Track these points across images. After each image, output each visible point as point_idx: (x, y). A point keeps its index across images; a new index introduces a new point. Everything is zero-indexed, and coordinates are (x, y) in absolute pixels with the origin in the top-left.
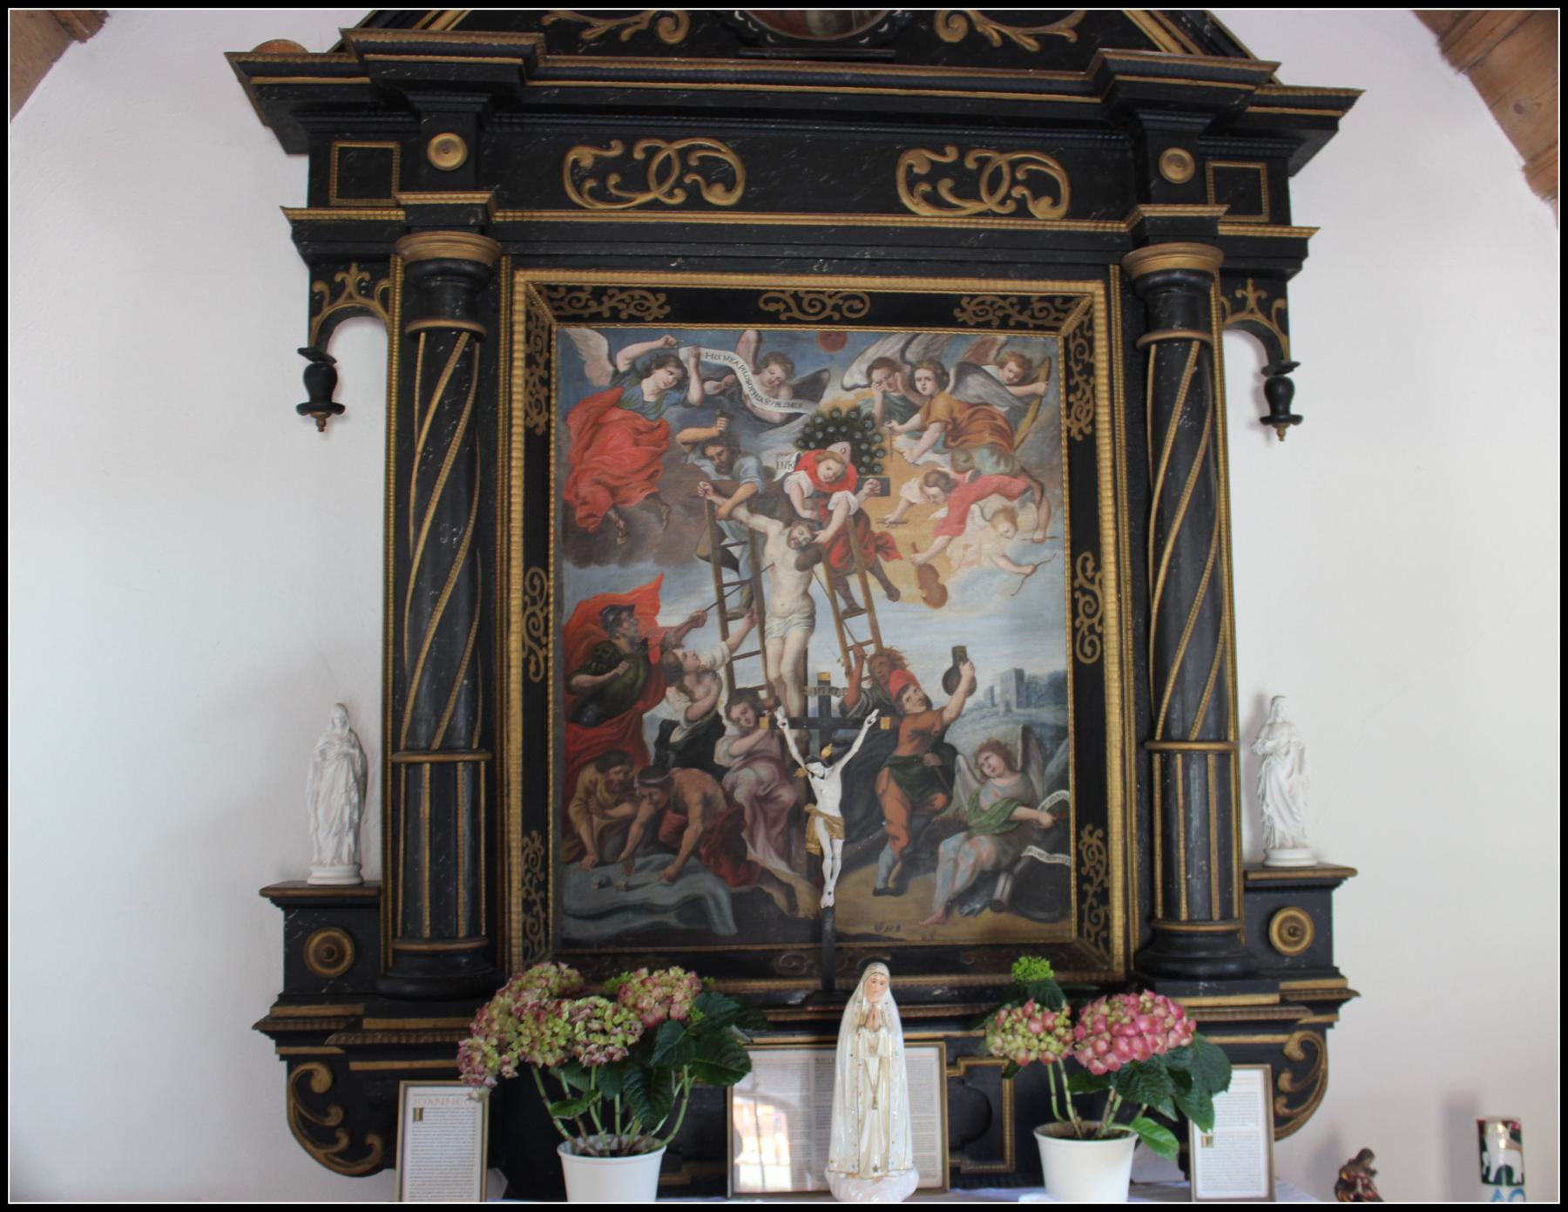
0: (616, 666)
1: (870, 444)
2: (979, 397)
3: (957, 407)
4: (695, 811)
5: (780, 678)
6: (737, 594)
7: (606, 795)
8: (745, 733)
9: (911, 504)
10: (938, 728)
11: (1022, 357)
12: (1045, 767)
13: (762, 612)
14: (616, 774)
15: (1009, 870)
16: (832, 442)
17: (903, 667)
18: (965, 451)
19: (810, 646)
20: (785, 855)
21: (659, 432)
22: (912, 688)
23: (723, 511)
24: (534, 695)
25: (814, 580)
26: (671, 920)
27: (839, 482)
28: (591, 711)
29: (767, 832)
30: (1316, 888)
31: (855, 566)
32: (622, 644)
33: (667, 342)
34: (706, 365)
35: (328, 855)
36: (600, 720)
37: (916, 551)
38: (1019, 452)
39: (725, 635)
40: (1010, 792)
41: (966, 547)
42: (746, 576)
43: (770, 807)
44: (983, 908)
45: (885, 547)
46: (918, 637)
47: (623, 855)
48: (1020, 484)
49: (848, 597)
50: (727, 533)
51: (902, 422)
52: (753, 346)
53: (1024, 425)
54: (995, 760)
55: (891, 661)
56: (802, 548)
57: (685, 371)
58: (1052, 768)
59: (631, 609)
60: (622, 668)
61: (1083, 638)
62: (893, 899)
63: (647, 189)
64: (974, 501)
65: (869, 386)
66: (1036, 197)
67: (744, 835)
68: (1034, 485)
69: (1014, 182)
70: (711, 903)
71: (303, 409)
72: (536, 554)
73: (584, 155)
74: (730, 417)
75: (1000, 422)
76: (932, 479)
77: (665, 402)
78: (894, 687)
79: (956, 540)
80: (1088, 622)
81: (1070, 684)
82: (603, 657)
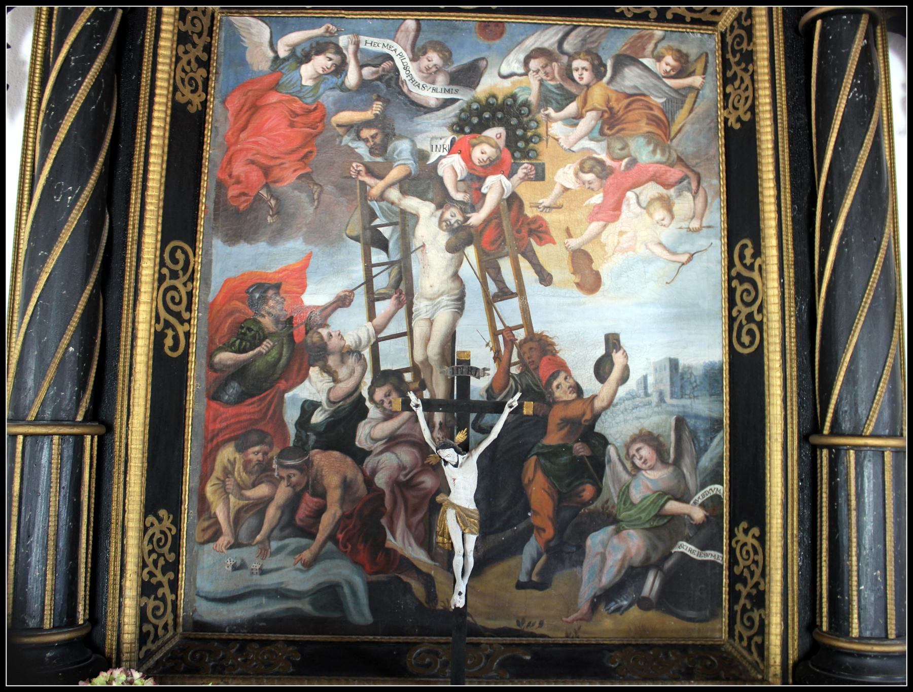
0: (260, 344)
1: (525, 130)
2: (636, 87)
3: (613, 97)
4: (334, 496)
6: (385, 274)
7: (244, 475)
8: (389, 416)
9: (566, 189)
10: (588, 416)
11: (679, 51)
13: (410, 293)
14: (255, 454)
15: (658, 566)
16: (487, 127)
17: (554, 353)
18: (621, 139)
19: (457, 329)
21: (316, 114)
22: (563, 375)
26: (305, 606)
27: (493, 166)
28: (233, 389)
31: (507, 249)
32: (267, 322)
33: (327, 30)
36: (242, 398)
37: (570, 236)
38: (675, 141)
39: (371, 315)
40: (662, 486)
41: (621, 233)
42: (395, 255)
43: (410, 494)
44: (630, 605)
45: (539, 231)
46: (571, 323)
48: (676, 173)
49: (499, 281)
50: (378, 213)
51: (559, 109)
52: (412, 35)
53: (681, 116)
54: (646, 452)
55: (542, 346)
56: (453, 230)
58: (706, 461)
59: (277, 287)
61: (741, 326)
62: (536, 593)
64: (630, 188)
65: (526, 74)
67: (384, 521)
68: (690, 174)
74: (387, 102)
75: (657, 113)
79: (611, 226)
81: (726, 375)
82: (247, 335)
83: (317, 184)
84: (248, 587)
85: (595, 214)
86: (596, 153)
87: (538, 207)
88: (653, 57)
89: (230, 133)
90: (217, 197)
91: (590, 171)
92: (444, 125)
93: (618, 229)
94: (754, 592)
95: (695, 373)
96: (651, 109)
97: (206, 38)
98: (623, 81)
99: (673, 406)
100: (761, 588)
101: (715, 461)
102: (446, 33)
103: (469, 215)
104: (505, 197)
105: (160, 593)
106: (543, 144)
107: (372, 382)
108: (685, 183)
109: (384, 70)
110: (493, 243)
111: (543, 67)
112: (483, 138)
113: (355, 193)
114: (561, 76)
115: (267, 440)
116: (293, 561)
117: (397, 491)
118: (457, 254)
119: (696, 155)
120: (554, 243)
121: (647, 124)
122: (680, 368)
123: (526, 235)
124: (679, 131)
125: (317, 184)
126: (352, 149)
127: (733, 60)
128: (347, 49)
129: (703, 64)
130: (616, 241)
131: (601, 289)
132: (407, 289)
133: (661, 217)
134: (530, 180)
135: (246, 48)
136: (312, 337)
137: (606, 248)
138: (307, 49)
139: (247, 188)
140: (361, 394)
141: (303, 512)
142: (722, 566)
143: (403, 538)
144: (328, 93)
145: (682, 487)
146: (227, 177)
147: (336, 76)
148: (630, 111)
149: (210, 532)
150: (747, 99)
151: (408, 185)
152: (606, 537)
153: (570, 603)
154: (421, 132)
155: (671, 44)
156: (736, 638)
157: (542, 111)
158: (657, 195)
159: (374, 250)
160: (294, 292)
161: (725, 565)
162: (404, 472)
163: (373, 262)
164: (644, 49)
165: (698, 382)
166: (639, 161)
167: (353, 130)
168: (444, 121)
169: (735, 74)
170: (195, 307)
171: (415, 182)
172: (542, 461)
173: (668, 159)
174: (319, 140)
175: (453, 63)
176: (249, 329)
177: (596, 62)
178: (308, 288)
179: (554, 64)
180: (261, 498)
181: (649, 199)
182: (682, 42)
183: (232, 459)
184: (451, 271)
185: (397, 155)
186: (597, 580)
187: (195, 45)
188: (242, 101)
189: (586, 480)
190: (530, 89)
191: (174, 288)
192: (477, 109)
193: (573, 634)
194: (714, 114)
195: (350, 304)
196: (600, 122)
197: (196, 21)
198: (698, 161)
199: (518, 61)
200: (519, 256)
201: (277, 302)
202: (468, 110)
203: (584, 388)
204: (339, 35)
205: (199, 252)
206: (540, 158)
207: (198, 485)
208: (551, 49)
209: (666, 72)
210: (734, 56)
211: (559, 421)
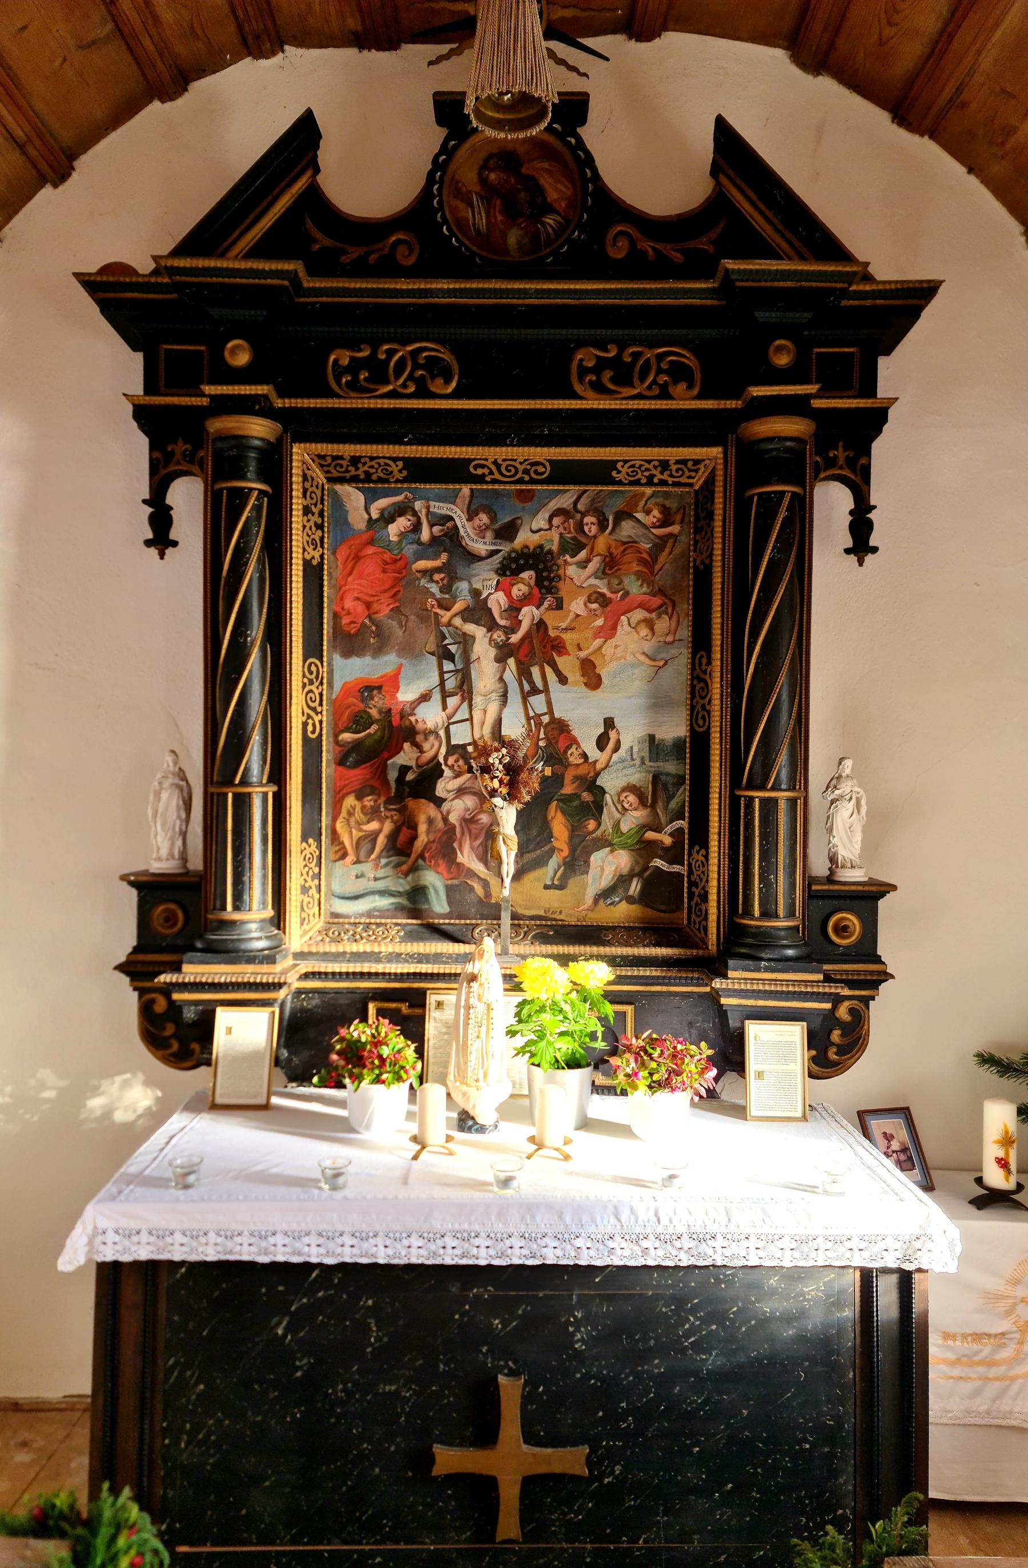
0: (369, 728)
1: (549, 572)
2: (630, 536)
3: (613, 544)
4: (422, 828)
6: (453, 678)
7: (362, 816)
8: (457, 775)
9: (578, 616)
10: (592, 774)
11: (663, 506)
12: (668, 803)
14: (369, 801)
15: (640, 875)
16: (523, 571)
17: (569, 732)
18: (618, 577)
20: (484, 860)
21: (400, 564)
22: (574, 747)
24: (312, 748)
29: (471, 844)
30: (868, 898)
32: (374, 712)
33: (406, 497)
34: (434, 514)
35: (164, 852)
37: (580, 649)
39: (445, 707)
40: (642, 821)
41: (616, 647)
42: (460, 666)
43: (473, 827)
44: (621, 901)
45: (559, 647)
46: (579, 709)
47: (373, 857)
48: (657, 601)
49: (531, 682)
53: (663, 558)
54: (632, 798)
55: (559, 728)
56: (499, 647)
57: (419, 519)
58: (673, 804)
59: (379, 688)
60: (374, 728)
61: (698, 712)
62: (557, 892)
63: (387, 382)
65: (550, 529)
66: (675, 383)
67: (455, 845)
69: (660, 371)
70: (432, 890)
71: (148, 543)
72: (313, 649)
73: (343, 357)
74: (451, 554)
75: (645, 555)
76: (593, 598)
78: (562, 745)
79: (609, 642)
82: (360, 721)
85: (598, 633)
97: (320, 506)
134: (553, 609)
141: (402, 838)
149: (340, 853)
151: (468, 615)
153: (580, 901)
170: (324, 703)
174: (404, 582)
176: (361, 717)
184: (497, 677)
205: (325, 664)
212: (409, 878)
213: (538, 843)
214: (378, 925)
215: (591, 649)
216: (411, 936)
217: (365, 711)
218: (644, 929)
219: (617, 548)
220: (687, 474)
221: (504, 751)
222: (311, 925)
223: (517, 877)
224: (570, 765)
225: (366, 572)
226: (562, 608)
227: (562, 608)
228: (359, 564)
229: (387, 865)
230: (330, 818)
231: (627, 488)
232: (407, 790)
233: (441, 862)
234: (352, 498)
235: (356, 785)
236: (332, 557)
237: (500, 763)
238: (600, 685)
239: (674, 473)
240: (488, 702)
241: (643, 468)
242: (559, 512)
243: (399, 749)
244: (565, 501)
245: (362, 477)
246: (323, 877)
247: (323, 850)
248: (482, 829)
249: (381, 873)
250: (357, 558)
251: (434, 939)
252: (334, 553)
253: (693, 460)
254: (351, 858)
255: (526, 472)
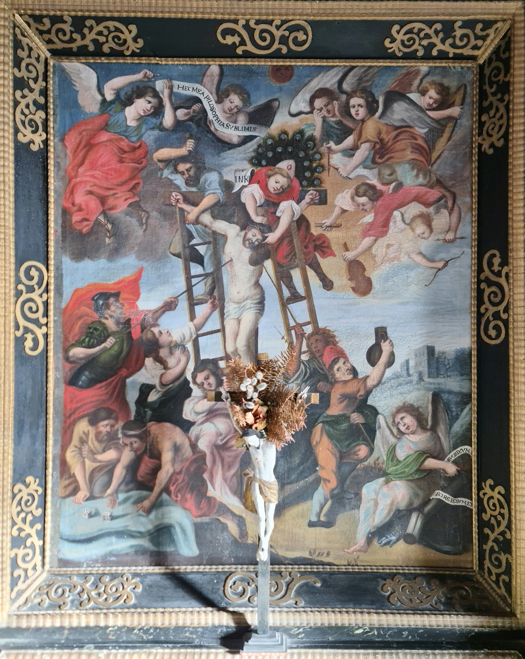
0: (105, 341)
1: (311, 161)
2: (403, 120)
3: (384, 129)
4: (167, 456)
5: (236, 352)
6: (203, 283)
7: (96, 443)
9: (344, 211)
10: (362, 393)
11: (441, 85)
12: (451, 426)
13: (222, 299)
14: (104, 426)
15: (420, 509)
16: (280, 160)
17: (335, 343)
18: (390, 166)
19: (259, 326)
21: (139, 152)
22: (342, 361)
23: (191, 217)
25: (264, 273)
27: (285, 193)
29: (224, 474)
31: (297, 261)
32: (111, 324)
33: (145, 76)
34: (178, 95)
37: (347, 250)
38: (435, 167)
39: (192, 317)
40: (422, 447)
41: (388, 246)
42: (209, 269)
43: (226, 454)
44: (398, 540)
45: (322, 246)
47: (109, 491)
48: (435, 193)
49: (291, 287)
50: (195, 234)
51: (338, 143)
52: (216, 79)
53: (441, 144)
54: (409, 420)
55: (325, 338)
57: (161, 101)
58: (458, 427)
59: (117, 295)
60: (110, 342)
61: (488, 322)
62: (324, 530)
64: (396, 208)
65: (311, 112)
67: (206, 476)
68: (447, 194)
70: (178, 529)
74: (198, 140)
75: (420, 142)
76: (361, 190)
77: (144, 128)
78: (327, 359)
79: (380, 241)
80: (493, 309)
81: (474, 359)
82: (95, 334)
83: (144, 211)
84: (101, 530)
85: (367, 231)
86: (368, 179)
87: (321, 226)
88: (419, 92)
89: (70, 168)
90: (64, 222)
91: (364, 195)
92: (245, 159)
93: (386, 243)
94: (501, 538)
95: (448, 357)
96: (416, 139)
97: (41, 83)
98: (392, 114)
99: (430, 384)
100: (508, 536)
101: (464, 427)
102: (244, 77)
103: (266, 235)
104: (295, 219)
105: (28, 543)
106: (325, 173)
107: (195, 369)
108: (442, 201)
109: (194, 111)
110: (286, 257)
111: (326, 106)
112: (276, 170)
113: (176, 218)
114: (341, 113)
115: (113, 416)
116: (136, 509)
117: (215, 451)
118: (258, 267)
119: (453, 177)
120: (335, 256)
121: (412, 152)
122: (436, 353)
123: (312, 249)
124: (439, 157)
125: (144, 211)
126: (171, 181)
127: (489, 91)
128: (163, 93)
129: (462, 96)
130: (384, 253)
131: (372, 292)
132: (219, 295)
133: (422, 231)
134: (315, 204)
135: (78, 91)
136: (146, 335)
137: (376, 259)
138: (129, 93)
139: (87, 214)
140: (186, 379)
141: (143, 469)
142: (472, 510)
143: (221, 489)
144: (149, 132)
145: (438, 448)
146: (71, 205)
147: (155, 117)
148: (398, 141)
149: (71, 488)
150: (501, 127)
151: (219, 211)
152: (378, 487)
153: (350, 539)
154: (227, 165)
155: (435, 78)
156: (486, 571)
157: (324, 144)
158: (418, 213)
159: (192, 264)
160: (130, 299)
161: (475, 510)
162: (220, 438)
163: (192, 274)
164: (411, 85)
165: (451, 364)
166: (405, 184)
167: (171, 164)
168: (245, 156)
169: (491, 104)
170: (51, 313)
171: (222, 208)
172: (327, 427)
173: (429, 182)
174: (144, 173)
175: (251, 104)
176: (96, 329)
177: (370, 99)
178: (141, 296)
179: (335, 102)
180: (110, 461)
181: (412, 217)
182: (444, 77)
183: (86, 431)
184: (253, 281)
185: (208, 186)
186: (371, 520)
187: (32, 90)
188: (78, 140)
189: (361, 442)
190: (314, 126)
191: (31, 300)
192: (272, 144)
193: (353, 563)
194: (469, 140)
195: (175, 308)
196: (373, 152)
197: (31, 68)
198: (453, 182)
199: (305, 101)
200: (307, 267)
201: (117, 307)
202: (263, 146)
203: (359, 371)
204: (156, 80)
205: (52, 268)
206: (323, 185)
207: (60, 452)
208: (332, 88)
209: (429, 105)
210: (491, 87)
211: (339, 397)
212: (152, 516)
213: (302, 472)
214: (114, 576)
215: (360, 249)
216: (151, 597)
217: (100, 322)
218: (428, 578)
219: (388, 133)
220: (473, 42)
221: (260, 375)
222: (28, 582)
223: (280, 511)
224: (336, 382)
225: (100, 162)
226: (325, 203)
227: (325, 203)
228: (91, 153)
229: (125, 500)
230: (59, 447)
231: (401, 63)
232: (149, 413)
233: (188, 496)
234: (83, 76)
235: (90, 409)
236: (60, 144)
237: (255, 389)
238: (370, 290)
239: (458, 43)
240: (242, 310)
241: (422, 35)
242: (322, 93)
243: (139, 366)
244: (328, 80)
245: (91, 48)
246: (48, 518)
247: (49, 485)
248: (236, 457)
249: (118, 510)
250: (90, 146)
251: (177, 599)
252: (63, 140)
253: (483, 21)
254: (83, 493)
255: (284, 40)
